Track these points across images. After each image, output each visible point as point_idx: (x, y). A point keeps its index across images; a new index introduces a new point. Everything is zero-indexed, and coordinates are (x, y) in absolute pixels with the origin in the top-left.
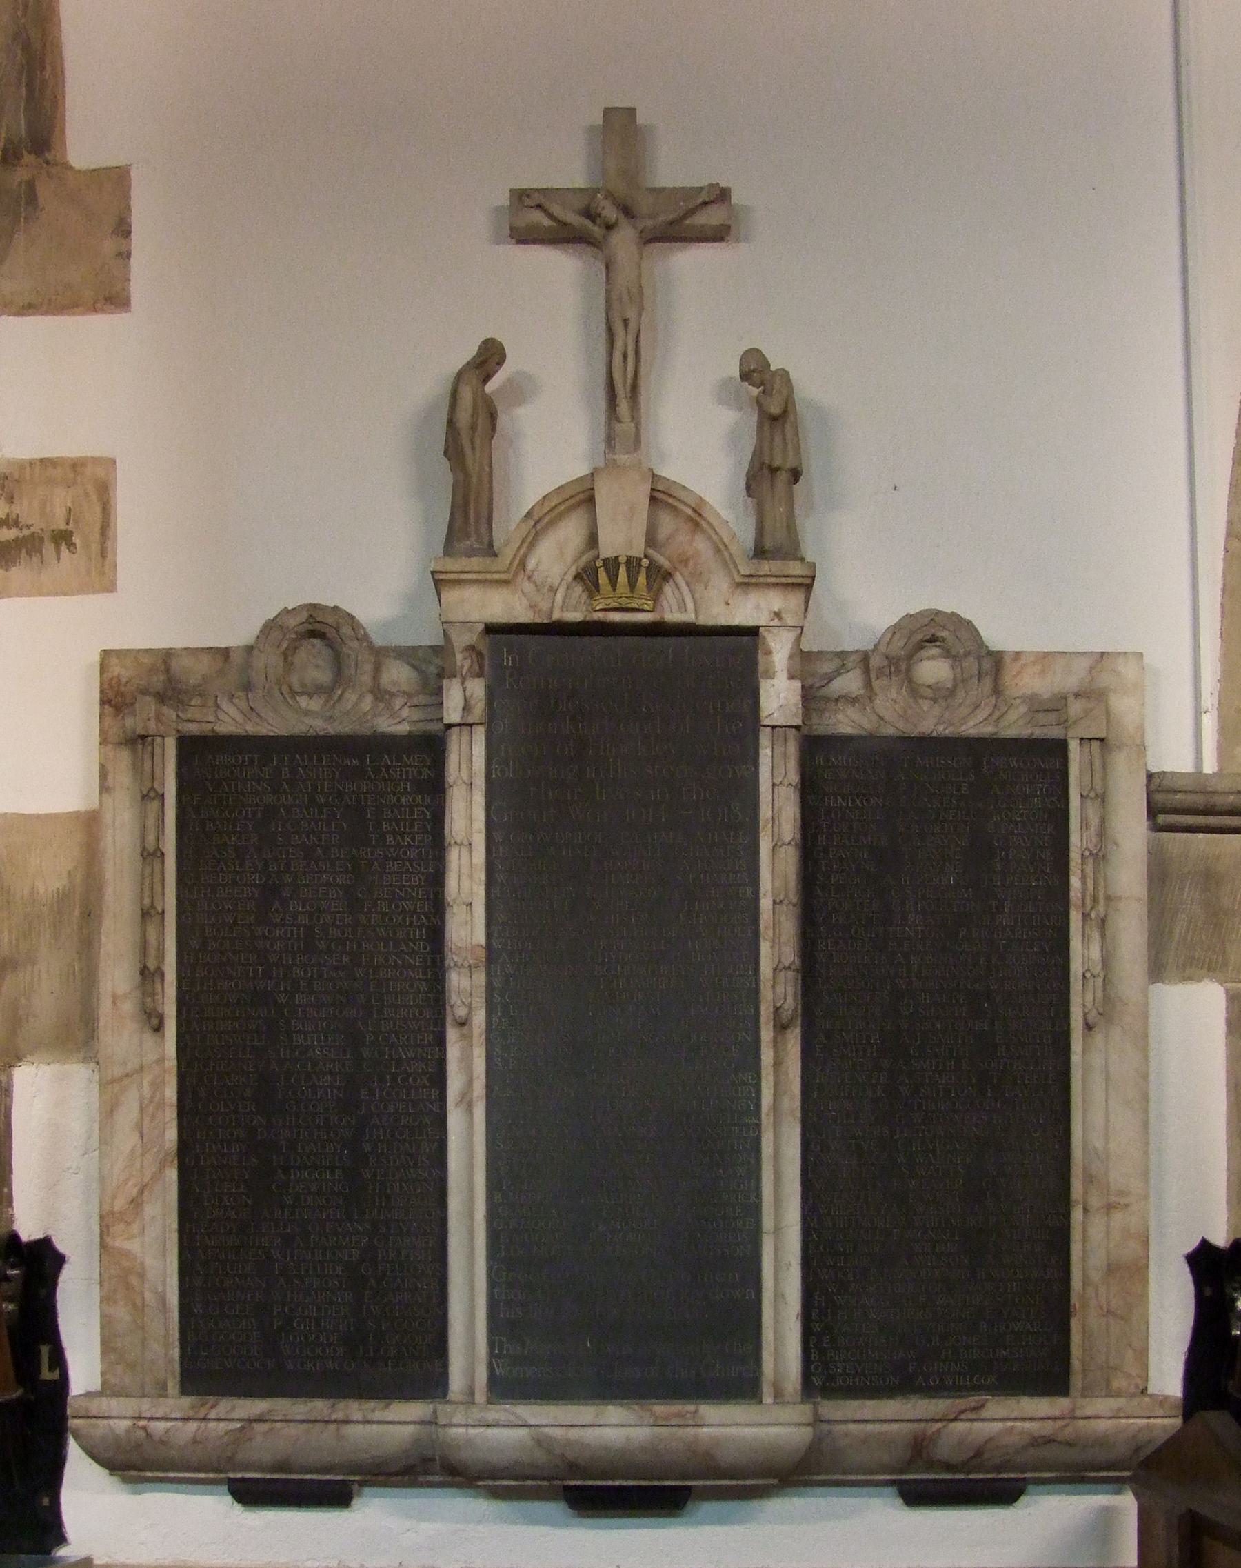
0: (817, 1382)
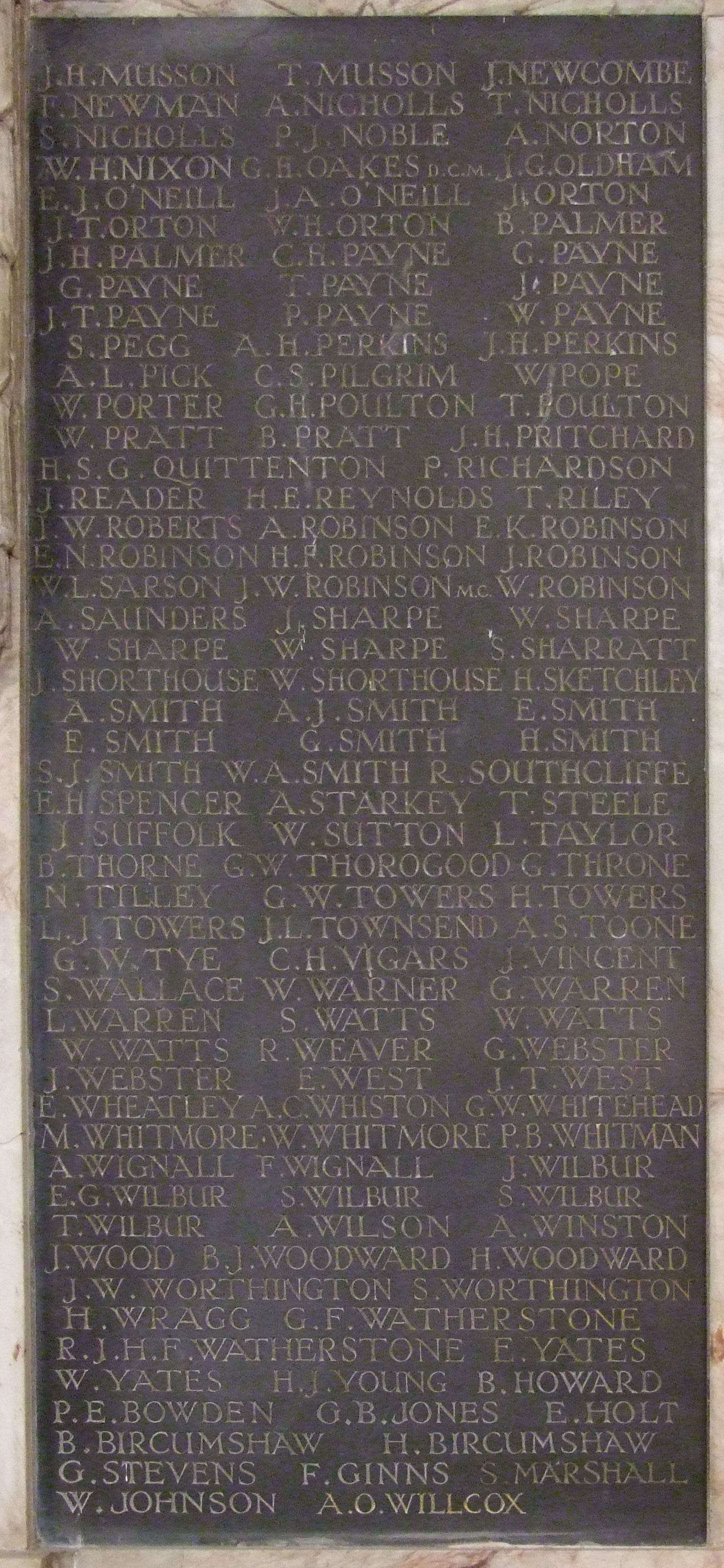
0: (75, 1503)
